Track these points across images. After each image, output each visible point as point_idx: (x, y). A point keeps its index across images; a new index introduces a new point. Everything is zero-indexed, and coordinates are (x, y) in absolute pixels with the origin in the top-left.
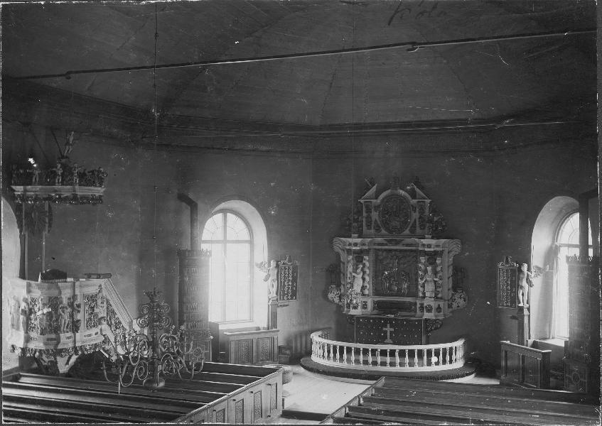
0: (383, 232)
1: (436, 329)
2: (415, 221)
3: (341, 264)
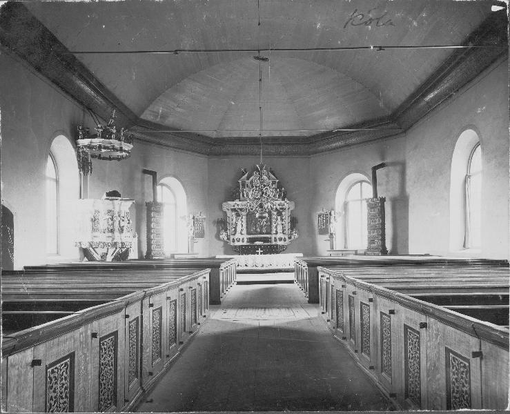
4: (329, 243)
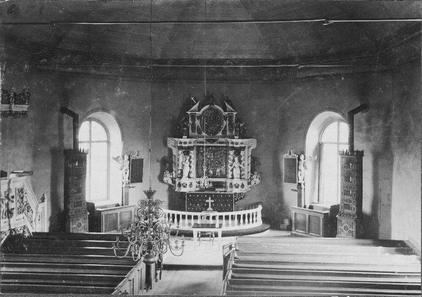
0: (204, 134)
1: (241, 199)
2: (226, 126)
3: (173, 156)
4: (296, 193)
